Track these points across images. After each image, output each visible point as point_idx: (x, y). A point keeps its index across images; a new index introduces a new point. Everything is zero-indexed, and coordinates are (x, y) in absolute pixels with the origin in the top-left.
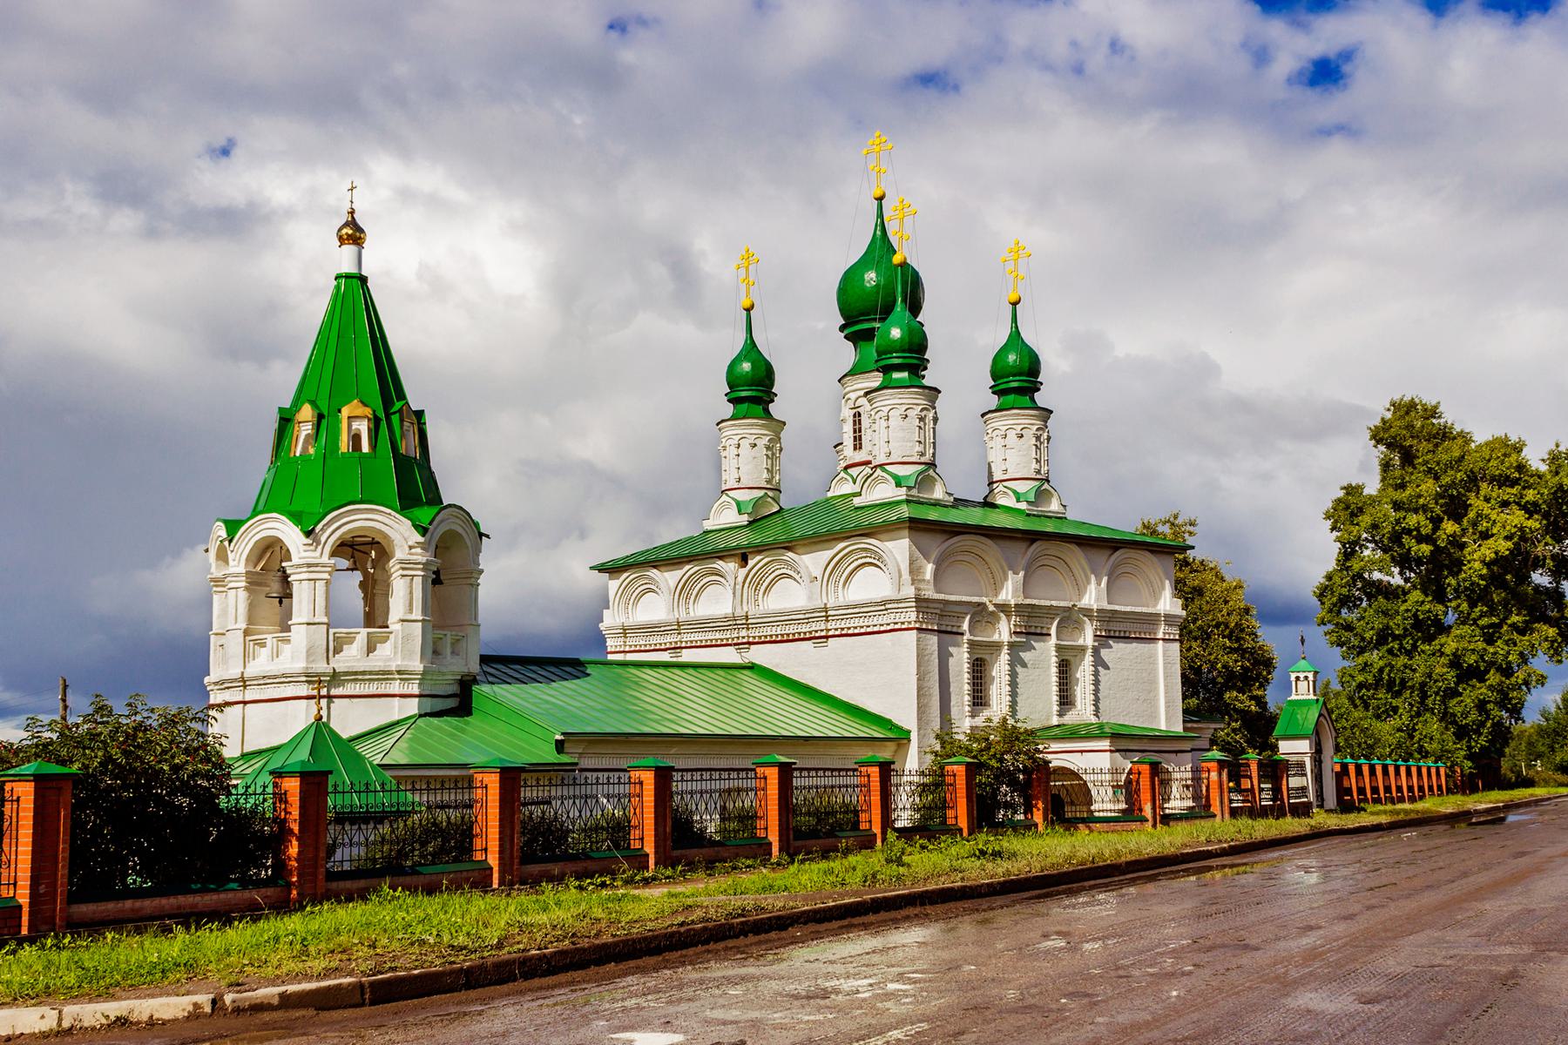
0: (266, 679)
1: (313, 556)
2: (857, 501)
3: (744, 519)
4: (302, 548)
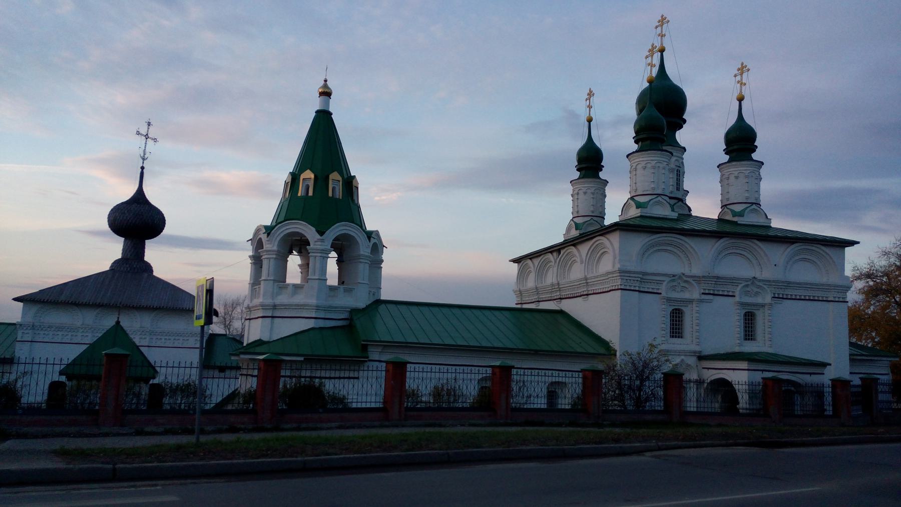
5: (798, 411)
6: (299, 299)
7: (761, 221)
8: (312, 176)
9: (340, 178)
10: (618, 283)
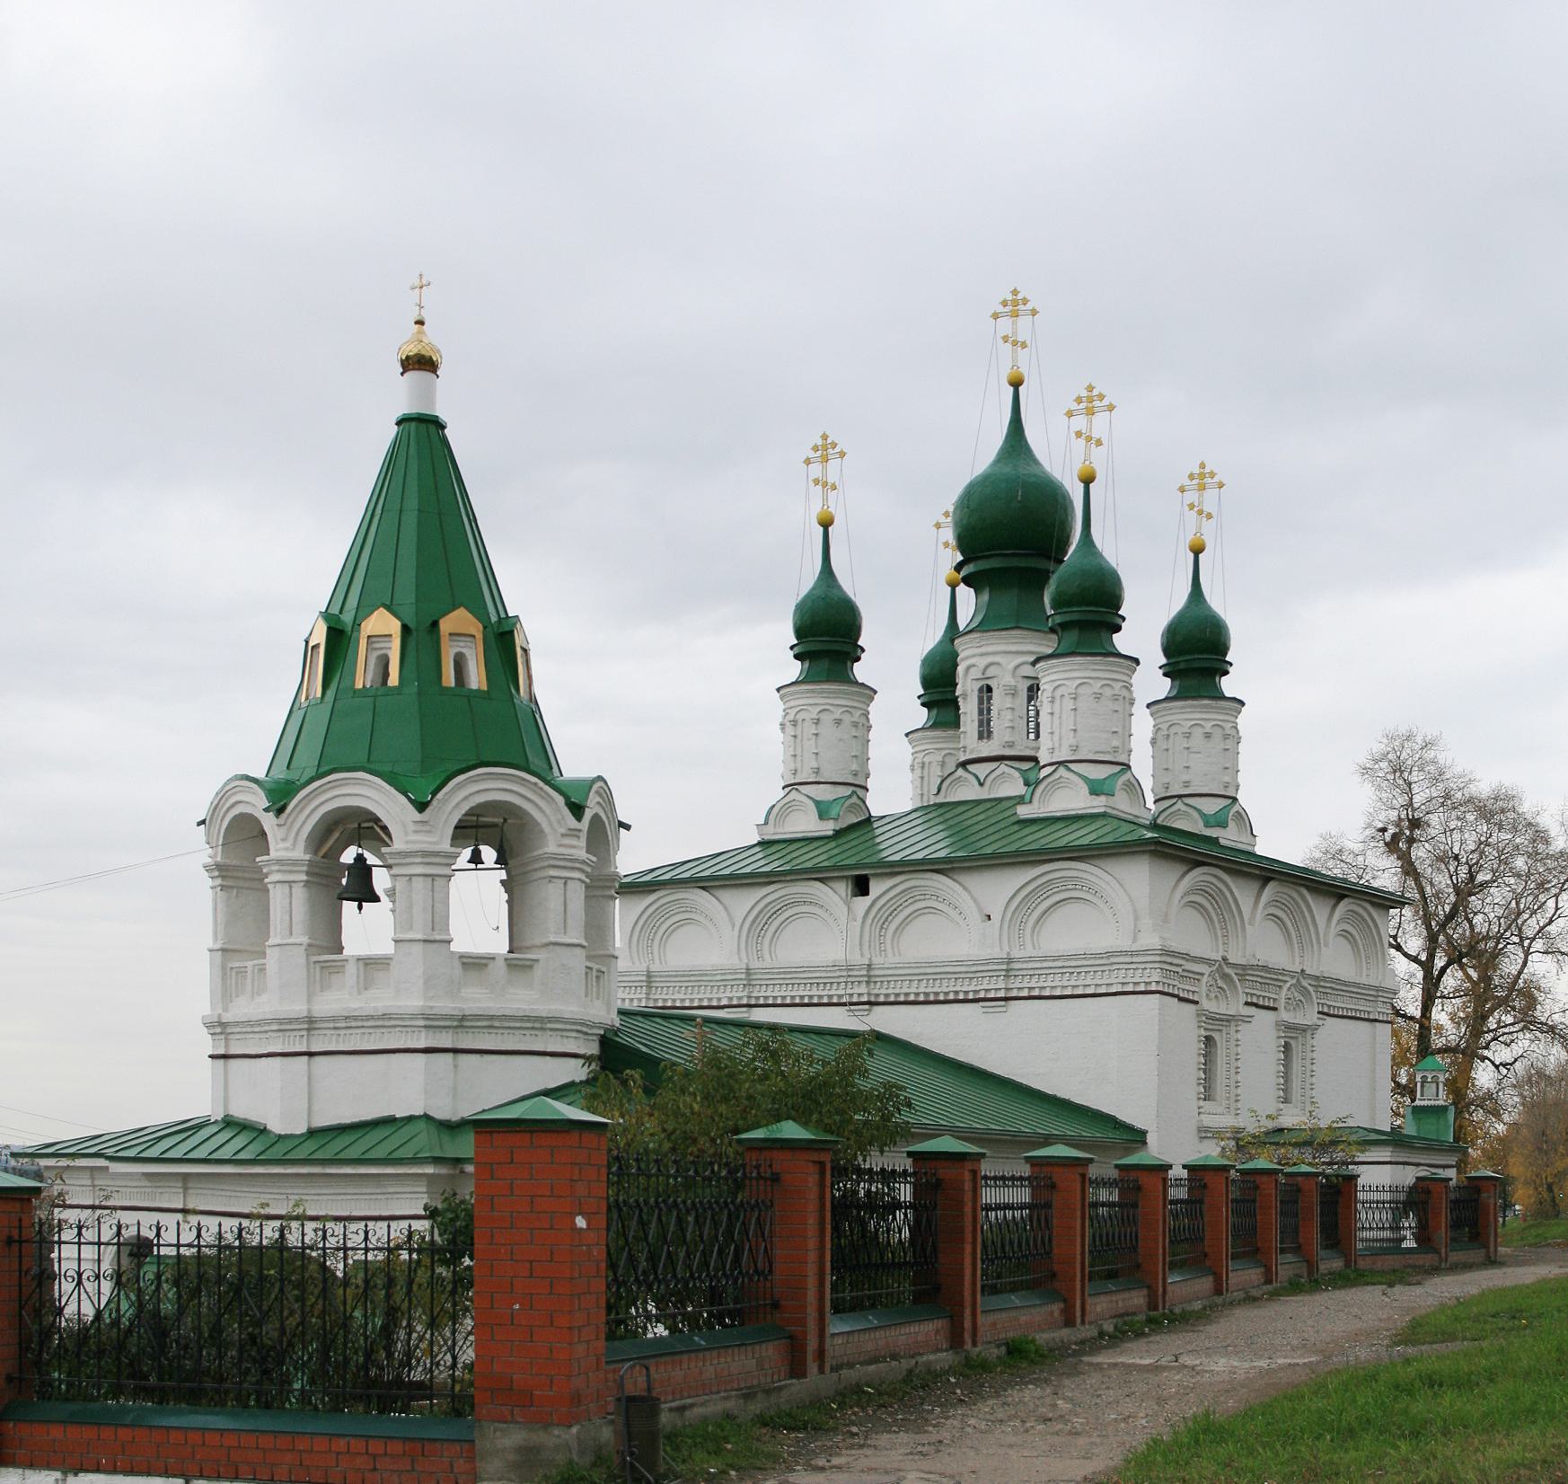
0: (350, 1021)
1: (424, 841)
2: (1023, 811)
3: (828, 828)
4: (412, 827)
5: (438, 1270)
6: (381, 999)
7: (1246, 838)
8: (394, 626)
9: (476, 628)
10: (593, 1049)
